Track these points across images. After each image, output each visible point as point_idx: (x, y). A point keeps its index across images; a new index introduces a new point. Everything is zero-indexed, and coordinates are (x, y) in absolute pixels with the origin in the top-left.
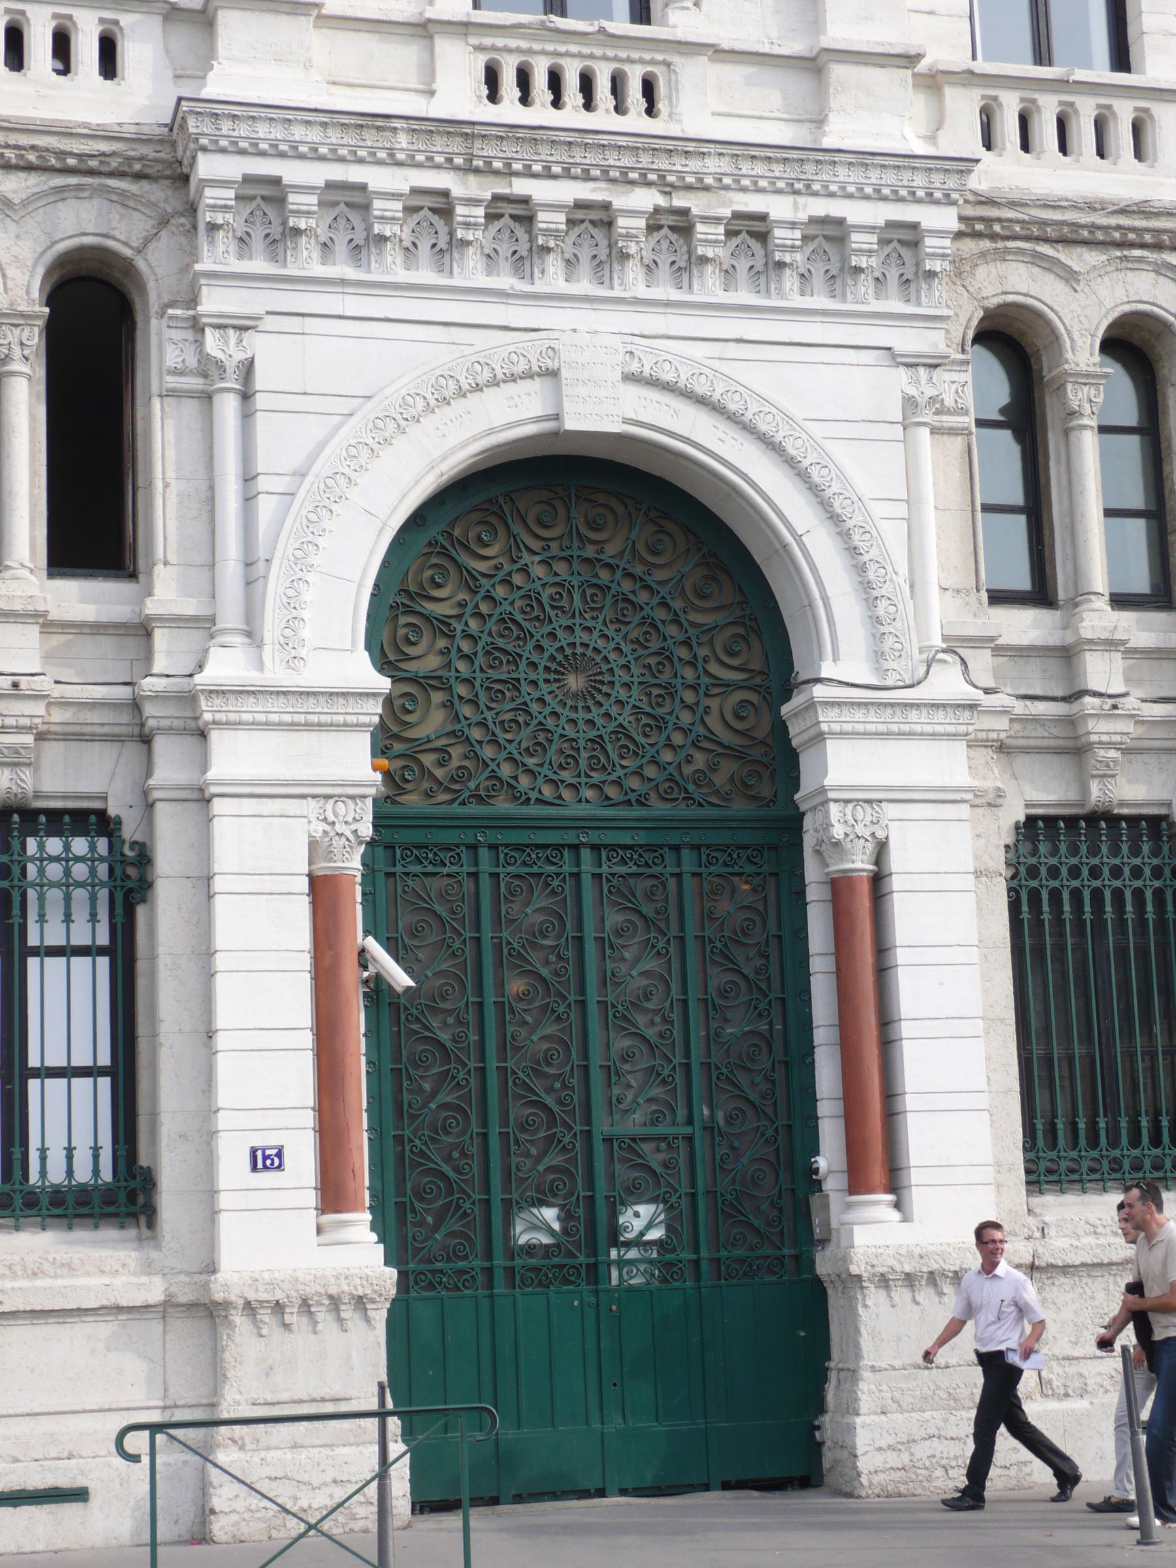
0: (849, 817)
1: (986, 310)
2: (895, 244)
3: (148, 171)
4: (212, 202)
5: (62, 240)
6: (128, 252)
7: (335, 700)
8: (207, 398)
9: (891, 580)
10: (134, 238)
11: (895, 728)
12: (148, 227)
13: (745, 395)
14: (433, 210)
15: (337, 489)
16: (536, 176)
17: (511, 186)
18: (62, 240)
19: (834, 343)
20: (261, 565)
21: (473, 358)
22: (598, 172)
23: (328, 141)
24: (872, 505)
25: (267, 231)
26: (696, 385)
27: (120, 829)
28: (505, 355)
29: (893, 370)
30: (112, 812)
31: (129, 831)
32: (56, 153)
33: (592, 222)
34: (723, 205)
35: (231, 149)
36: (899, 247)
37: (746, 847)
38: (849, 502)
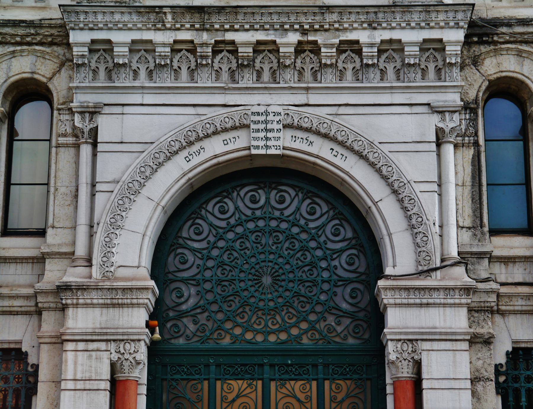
0: (399, 349)
1: (489, 81)
2: (431, 51)
3: (55, 41)
4: (449, 52)
5: (14, 76)
6: (44, 80)
7: (126, 292)
8: (77, 146)
9: (425, 224)
10: (48, 73)
11: (425, 301)
12: (54, 67)
13: (347, 132)
14: (187, 50)
15: (134, 188)
16: (237, 30)
17: (224, 35)
18: (14, 76)
19: (398, 103)
20: (95, 226)
21: (206, 121)
22: (268, 26)
23: (132, 21)
24: (413, 184)
25: (107, 66)
26: (322, 129)
27: (27, 358)
28: (222, 119)
29: (431, 115)
30: (24, 350)
31: (32, 360)
32: (10, 35)
33: (268, 51)
34: (335, 38)
35: (134, 28)
36: (434, 52)
37: (353, 365)
38: (403, 184)
